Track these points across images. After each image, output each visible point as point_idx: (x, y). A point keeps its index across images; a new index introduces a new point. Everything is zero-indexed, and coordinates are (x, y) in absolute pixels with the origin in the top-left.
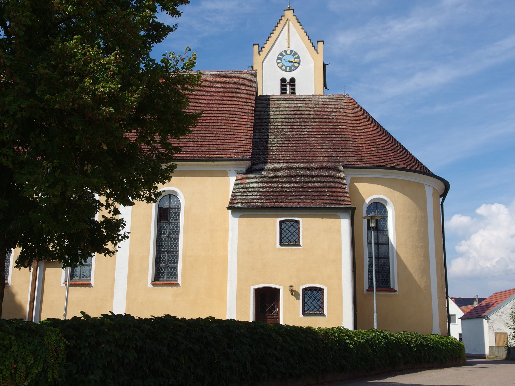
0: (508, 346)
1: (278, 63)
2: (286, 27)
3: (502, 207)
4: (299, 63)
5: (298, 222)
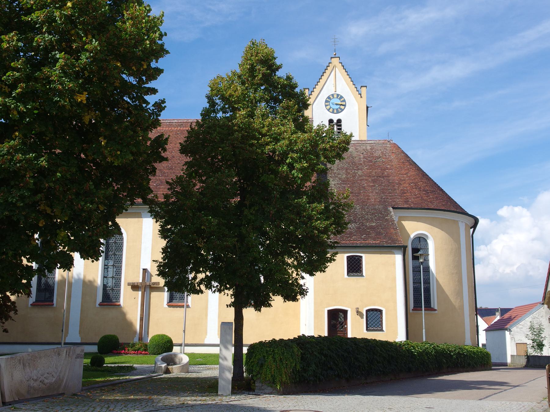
0: (527, 355)
1: (326, 106)
2: (333, 73)
3: (525, 211)
4: (345, 106)
5: (361, 257)
